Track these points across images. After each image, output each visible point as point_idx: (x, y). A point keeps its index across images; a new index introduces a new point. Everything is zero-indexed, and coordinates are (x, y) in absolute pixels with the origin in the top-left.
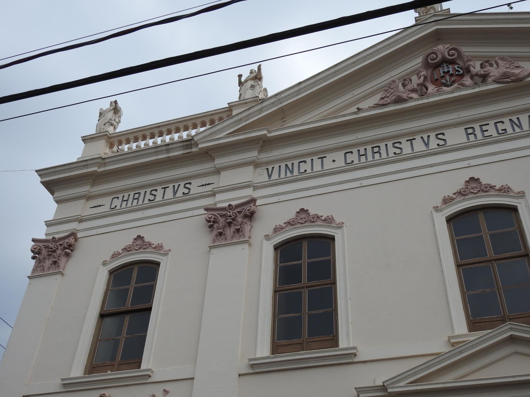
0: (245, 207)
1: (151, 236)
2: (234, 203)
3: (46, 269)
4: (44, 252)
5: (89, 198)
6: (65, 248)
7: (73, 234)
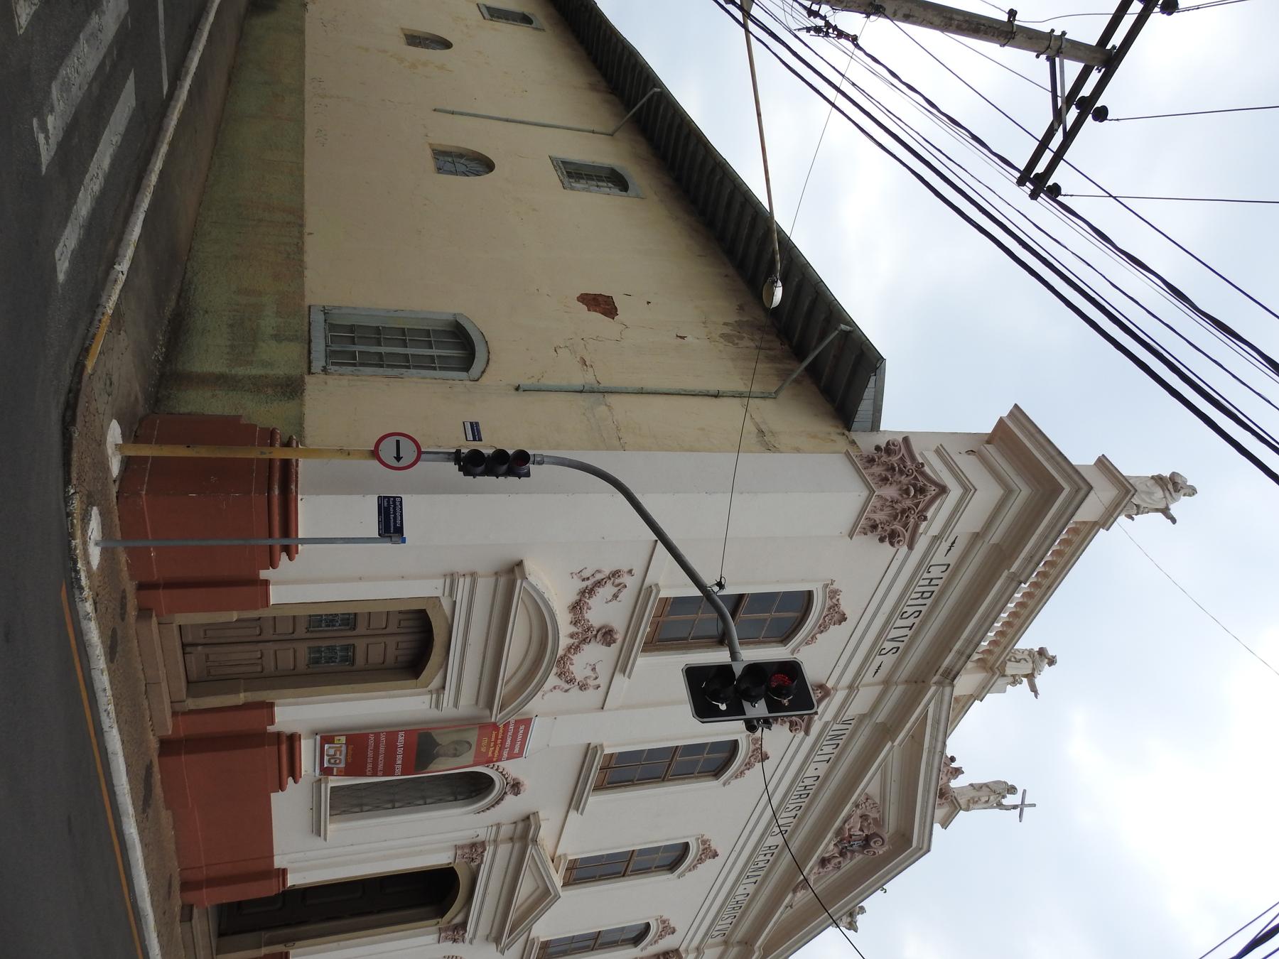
0: (907, 535)
1: (836, 633)
2: (926, 469)
3: (871, 471)
4: (894, 459)
5: (976, 537)
6: (914, 486)
7: (911, 547)
